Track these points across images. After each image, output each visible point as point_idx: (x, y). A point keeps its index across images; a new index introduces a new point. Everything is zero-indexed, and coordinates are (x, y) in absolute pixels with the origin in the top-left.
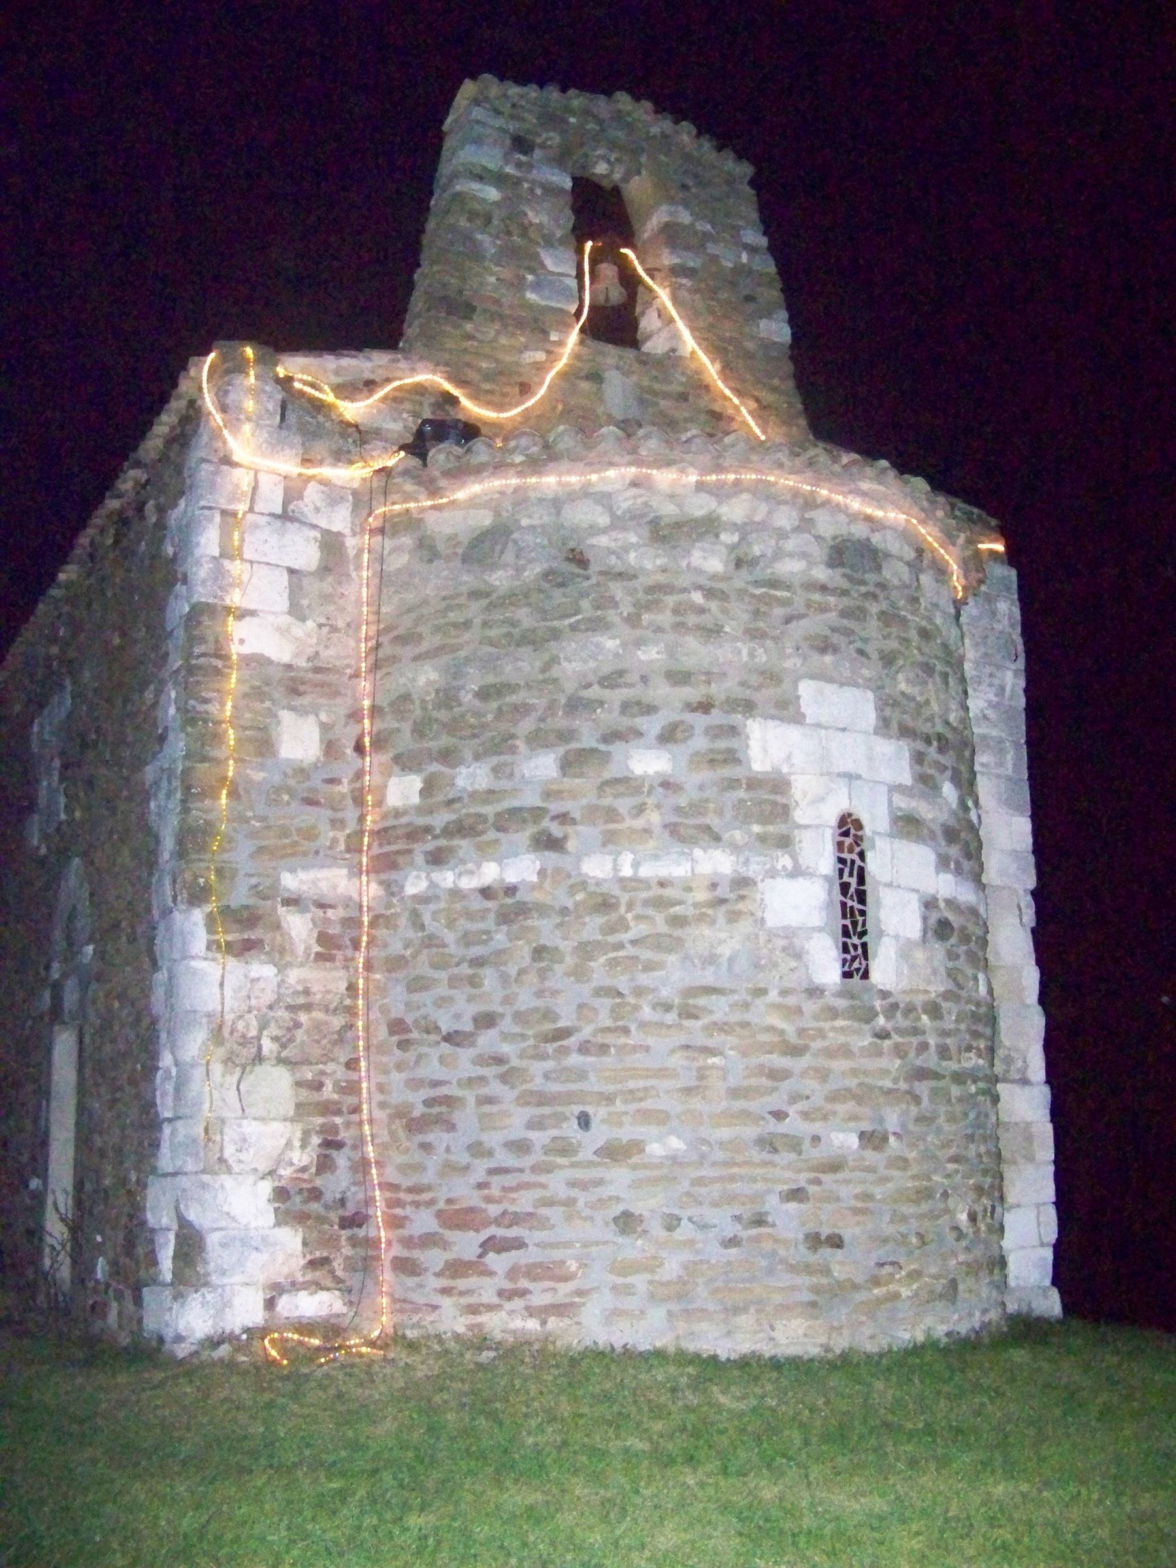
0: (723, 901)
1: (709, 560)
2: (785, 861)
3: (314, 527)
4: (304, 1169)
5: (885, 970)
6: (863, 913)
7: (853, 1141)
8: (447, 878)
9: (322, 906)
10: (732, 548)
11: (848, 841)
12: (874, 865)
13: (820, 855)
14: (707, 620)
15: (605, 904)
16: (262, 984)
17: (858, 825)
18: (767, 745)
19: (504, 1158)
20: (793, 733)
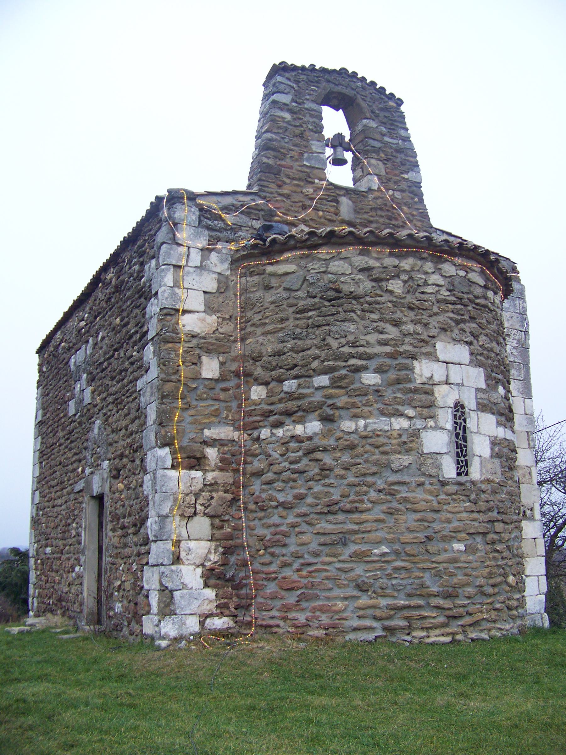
0: (405, 443)
1: (396, 286)
3: (215, 272)
5: (475, 473)
6: (465, 446)
8: (280, 432)
10: (405, 282)
11: (459, 414)
12: (471, 424)
13: (446, 419)
17: (463, 407)
18: (423, 369)
19: (309, 559)
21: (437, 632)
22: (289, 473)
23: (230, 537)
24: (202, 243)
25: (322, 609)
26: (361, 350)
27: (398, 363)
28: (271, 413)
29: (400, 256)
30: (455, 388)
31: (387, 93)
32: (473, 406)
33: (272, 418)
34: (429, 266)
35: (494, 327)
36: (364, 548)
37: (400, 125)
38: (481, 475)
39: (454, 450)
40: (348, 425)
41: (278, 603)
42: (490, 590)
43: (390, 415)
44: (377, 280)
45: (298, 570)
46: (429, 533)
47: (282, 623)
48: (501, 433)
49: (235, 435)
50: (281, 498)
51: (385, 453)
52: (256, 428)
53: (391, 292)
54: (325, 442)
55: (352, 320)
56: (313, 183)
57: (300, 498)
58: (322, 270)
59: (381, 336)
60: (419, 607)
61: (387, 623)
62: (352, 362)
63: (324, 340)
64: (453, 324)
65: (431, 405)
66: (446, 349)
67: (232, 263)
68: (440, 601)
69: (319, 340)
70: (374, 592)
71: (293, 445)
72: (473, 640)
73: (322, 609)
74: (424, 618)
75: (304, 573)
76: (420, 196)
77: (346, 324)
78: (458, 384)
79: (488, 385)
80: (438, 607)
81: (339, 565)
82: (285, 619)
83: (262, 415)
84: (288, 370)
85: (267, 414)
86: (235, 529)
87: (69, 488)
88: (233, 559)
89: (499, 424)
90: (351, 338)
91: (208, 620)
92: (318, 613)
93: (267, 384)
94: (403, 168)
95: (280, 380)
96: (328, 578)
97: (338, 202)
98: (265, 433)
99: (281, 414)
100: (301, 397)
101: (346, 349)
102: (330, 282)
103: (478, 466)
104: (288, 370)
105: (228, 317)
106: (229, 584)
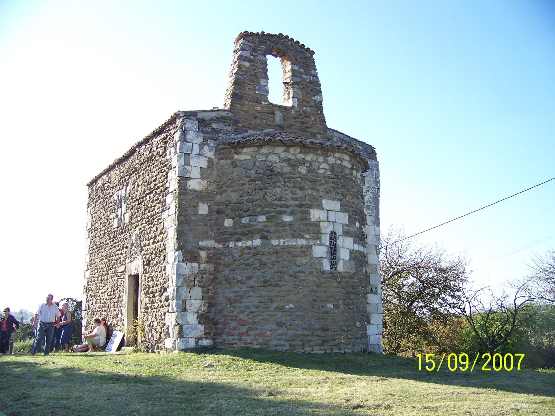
0: (304, 251)
1: (303, 170)
2: (318, 242)
3: (206, 157)
4: (204, 311)
5: (340, 267)
6: (336, 254)
7: (332, 306)
8: (239, 244)
9: (209, 250)
10: (308, 167)
11: (333, 237)
12: (339, 243)
13: (326, 240)
14: (302, 185)
15: (277, 252)
16: (194, 268)
17: (335, 234)
18: (315, 214)
19: (253, 309)
20: (321, 212)
21: (317, 348)
22: (244, 265)
23: (212, 297)
24: (200, 140)
25: (260, 335)
26: (283, 203)
27: (303, 209)
28: (236, 233)
29: (305, 153)
30: (332, 224)
31: (306, 47)
32: (341, 233)
33: (236, 237)
34: (321, 159)
35: (355, 190)
36: (282, 304)
37: (312, 67)
38: (344, 269)
39: (329, 256)
40: (275, 242)
41: (236, 332)
42: (346, 329)
43: (297, 237)
44: (293, 166)
45: (248, 315)
46: (315, 298)
47: (238, 342)
48: (356, 247)
49: (216, 245)
50: (239, 278)
51: (294, 256)
52: (227, 241)
53: (300, 173)
54: (263, 250)
55: (279, 187)
56: (261, 103)
57: (249, 278)
58: (264, 159)
59: (294, 196)
60: (308, 335)
61: (291, 343)
62: (278, 209)
63: (264, 197)
64: (332, 189)
65: (319, 232)
66: (326, 203)
67: (215, 152)
68: (319, 333)
69: (261, 197)
70: (286, 327)
71: (246, 251)
72: (335, 353)
73: (260, 335)
74: (311, 341)
75: (251, 317)
76: (321, 109)
77: (276, 189)
78: (333, 222)
79: (350, 222)
80: (318, 336)
81: (269, 313)
82: (240, 340)
83: (230, 235)
84: (244, 212)
85: (233, 234)
86: (215, 293)
87: (113, 270)
88: (213, 310)
89: (355, 242)
90: (278, 196)
91: (200, 341)
92: (257, 337)
93: (233, 218)
94: (313, 93)
95: (241, 217)
96: (262, 319)
97: (274, 114)
98: (231, 245)
99: (240, 234)
100: (250, 226)
101: (275, 202)
102: (268, 166)
103: (342, 264)
104: (244, 212)
105: (213, 181)
106: (211, 322)
